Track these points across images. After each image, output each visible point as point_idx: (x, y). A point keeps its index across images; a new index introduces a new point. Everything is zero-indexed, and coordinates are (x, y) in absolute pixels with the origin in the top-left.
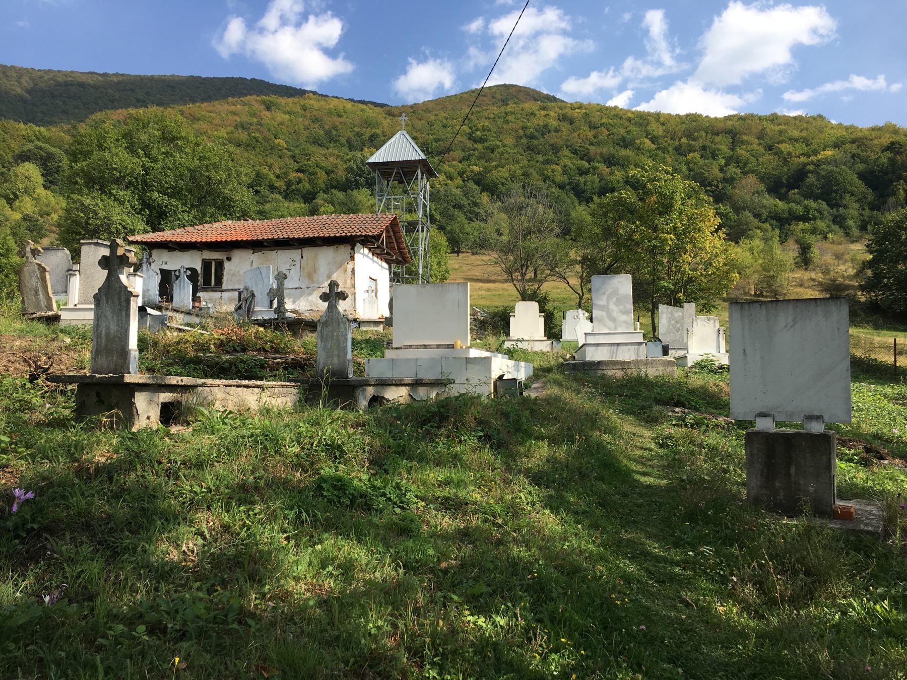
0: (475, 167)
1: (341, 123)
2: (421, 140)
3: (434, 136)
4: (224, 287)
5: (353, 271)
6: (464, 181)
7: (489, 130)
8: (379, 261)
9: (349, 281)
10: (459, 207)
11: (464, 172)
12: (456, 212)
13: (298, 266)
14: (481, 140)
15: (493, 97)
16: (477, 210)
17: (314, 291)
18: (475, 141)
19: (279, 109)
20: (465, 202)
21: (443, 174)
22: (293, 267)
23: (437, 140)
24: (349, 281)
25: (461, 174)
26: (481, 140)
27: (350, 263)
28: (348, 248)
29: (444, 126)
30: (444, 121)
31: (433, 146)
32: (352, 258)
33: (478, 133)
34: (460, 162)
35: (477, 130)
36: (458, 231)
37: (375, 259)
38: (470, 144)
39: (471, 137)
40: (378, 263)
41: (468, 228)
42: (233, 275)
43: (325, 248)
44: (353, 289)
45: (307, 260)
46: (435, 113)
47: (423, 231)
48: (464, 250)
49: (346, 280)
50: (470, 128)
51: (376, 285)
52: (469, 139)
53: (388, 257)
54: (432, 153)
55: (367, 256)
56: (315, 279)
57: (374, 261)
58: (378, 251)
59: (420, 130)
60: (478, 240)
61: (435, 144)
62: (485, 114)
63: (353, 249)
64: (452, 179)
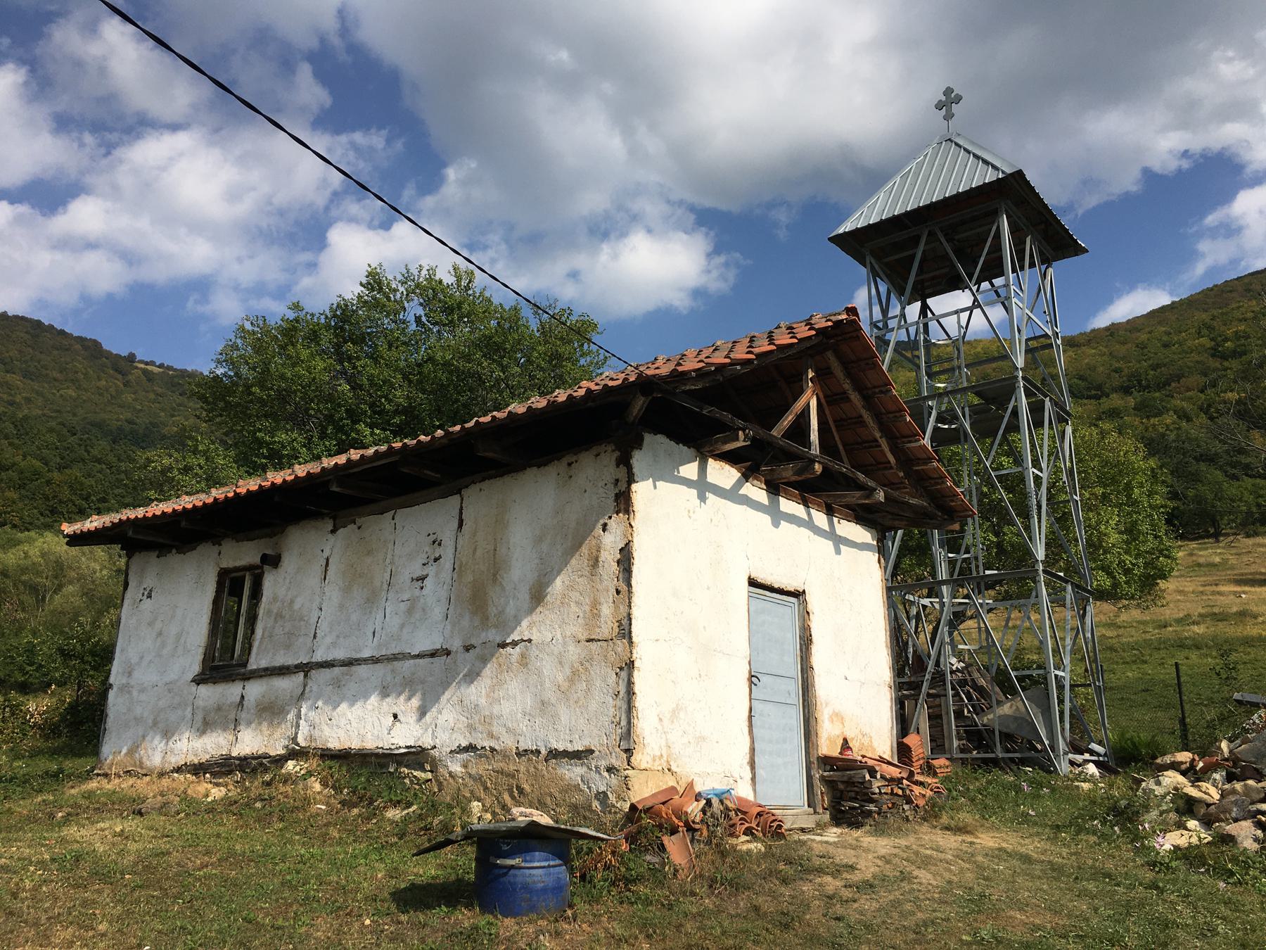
0: (1230, 395)
1: (994, 370)
2: (1126, 370)
3: (1151, 362)
4: (257, 661)
5: (626, 559)
6: (1212, 419)
7: (1248, 337)
8: (820, 518)
9: (606, 610)
10: (1211, 459)
11: (1209, 406)
12: (1203, 466)
13: (447, 563)
14: (1235, 354)
15: (1249, 290)
16: (1244, 460)
17: (484, 660)
18: (1224, 357)
19: (903, 367)
20: (1218, 447)
21: (1171, 413)
22: (431, 570)
23: (1155, 367)
24: (606, 610)
25: (1205, 409)
26: (1235, 354)
27: (612, 524)
28: (609, 458)
29: (1166, 346)
30: (1165, 338)
31: (1149, 377)
32: (623, 503)
33: (1228, 344)
34: (1202, 391)
35: (1226, 340)
36: (1210, 496)
37: (788, 506)
38: (1214, 363)
39: (1215, 353)
40: (810, 525)
41: (1231, 489)
42: (279, 616)
43: (531, 473)
44: (621, 645)
45: (474, 534)
46: (1147, 330)
47: (1038, 423)
48: (1229, 531)
49: (595, 604)
50: (1212, 339)
51: (805, 614)
52: (1213, 356)
53: (855, 497)
54: (1148, 387)
55: (731, 495)
56: (492, 611)
57: (778, 517)
58: (788, 471)
59: (1123, 358)
60: (1254, 509)
61: (1152, 372)
62: (1238, 314)
63: (624, 461)
64: (1189, 420)
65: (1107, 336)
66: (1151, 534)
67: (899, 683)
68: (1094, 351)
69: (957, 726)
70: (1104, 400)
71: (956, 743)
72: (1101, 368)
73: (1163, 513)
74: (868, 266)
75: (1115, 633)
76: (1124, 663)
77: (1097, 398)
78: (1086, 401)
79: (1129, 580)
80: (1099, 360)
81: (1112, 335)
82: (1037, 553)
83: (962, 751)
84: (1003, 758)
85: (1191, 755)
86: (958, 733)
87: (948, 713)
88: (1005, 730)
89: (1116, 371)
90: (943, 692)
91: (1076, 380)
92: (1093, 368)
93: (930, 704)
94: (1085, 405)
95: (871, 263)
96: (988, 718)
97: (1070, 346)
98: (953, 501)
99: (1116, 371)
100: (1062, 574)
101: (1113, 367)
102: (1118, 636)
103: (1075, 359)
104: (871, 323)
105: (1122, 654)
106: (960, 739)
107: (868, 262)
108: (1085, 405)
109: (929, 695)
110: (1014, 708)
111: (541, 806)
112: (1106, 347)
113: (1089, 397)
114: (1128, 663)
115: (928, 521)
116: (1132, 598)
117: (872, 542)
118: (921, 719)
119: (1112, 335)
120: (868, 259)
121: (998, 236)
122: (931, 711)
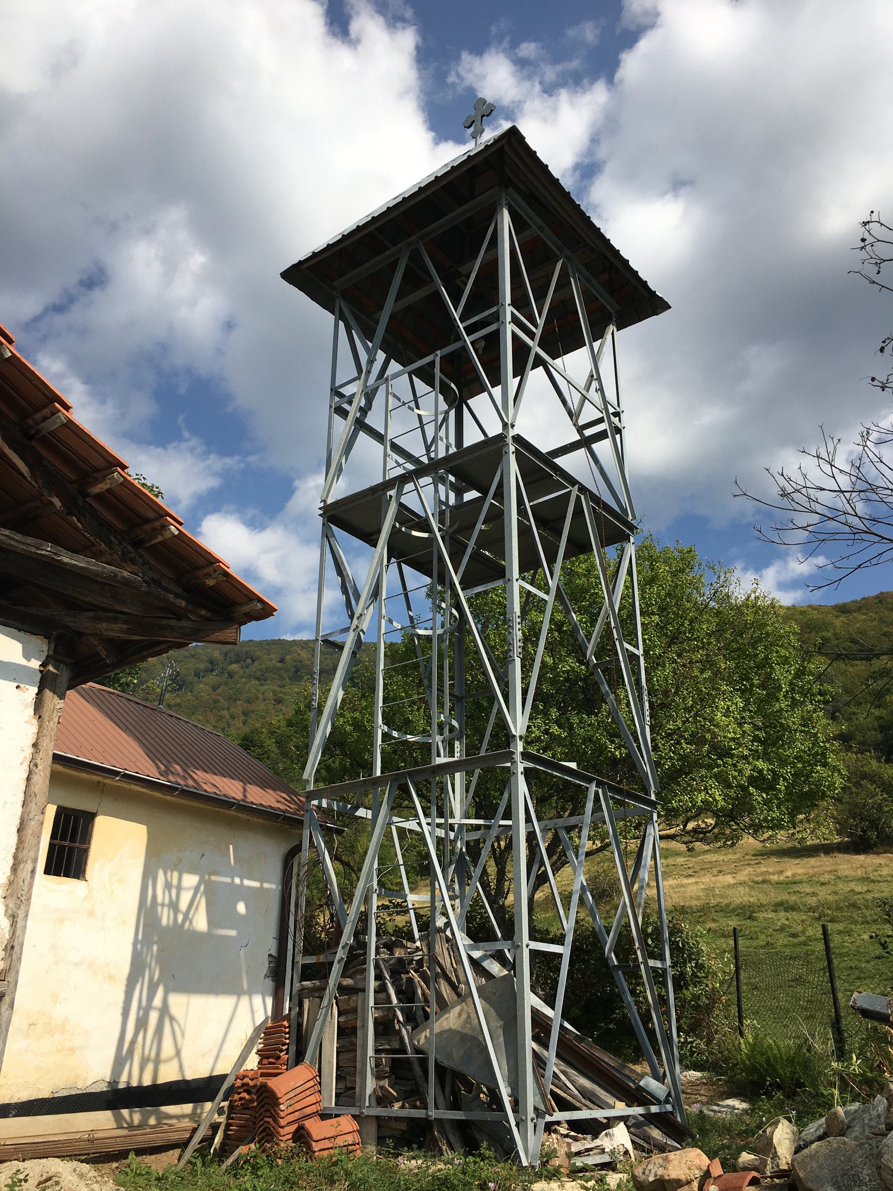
65: (876, 603)
66: (801, 731)
67: (365, 964)
68: (864, 617)
69: (377, 1051)
70: (874, 661)
71: (371, 1084)
72: (872, 633)
73: (819, 701)
74: (337, 312)
75: (865, 888)
76: (863, 923)
77: (868, 659)
78: (858, 662)
79: (770, 800)
80: (870, 624)
81: (881, 602)
82: (515, 723)
83: (382, 1100)
84: (439, 1121)
85: (704, 1161)
86: (377, 1065)
87: (365, 1027)
88: (445, 1063)
89: (885, 635)
90: (360, 986)
91: (848, 643)
92: (863, 632)
93: (344, 1007)
94: (857, 665)
95: (340, 309)
96: (422, 1038)
97: (843, 612)
98: (208, 575)
99: (885, 635)
100: (573, 765)
101: (883, 631)
102: (868, 891)
103: (848, 624)
104: (332, 390)
105: (865, 911)
106: (378, 1077)
107: (337, 307)
108: (857, 665)
109: (341, 989)
110: (464, 1016)
111: (148, 1110)
112: (876, 613)
113: (862, 659)
114: (867, 923)
115: (173, 622)
116: (780, 827)
117: (23, 662)
118: (327, 1030)
119: (881, 602)
120: (340, 303)
121: (495, 242)
122: (342, 1019)
